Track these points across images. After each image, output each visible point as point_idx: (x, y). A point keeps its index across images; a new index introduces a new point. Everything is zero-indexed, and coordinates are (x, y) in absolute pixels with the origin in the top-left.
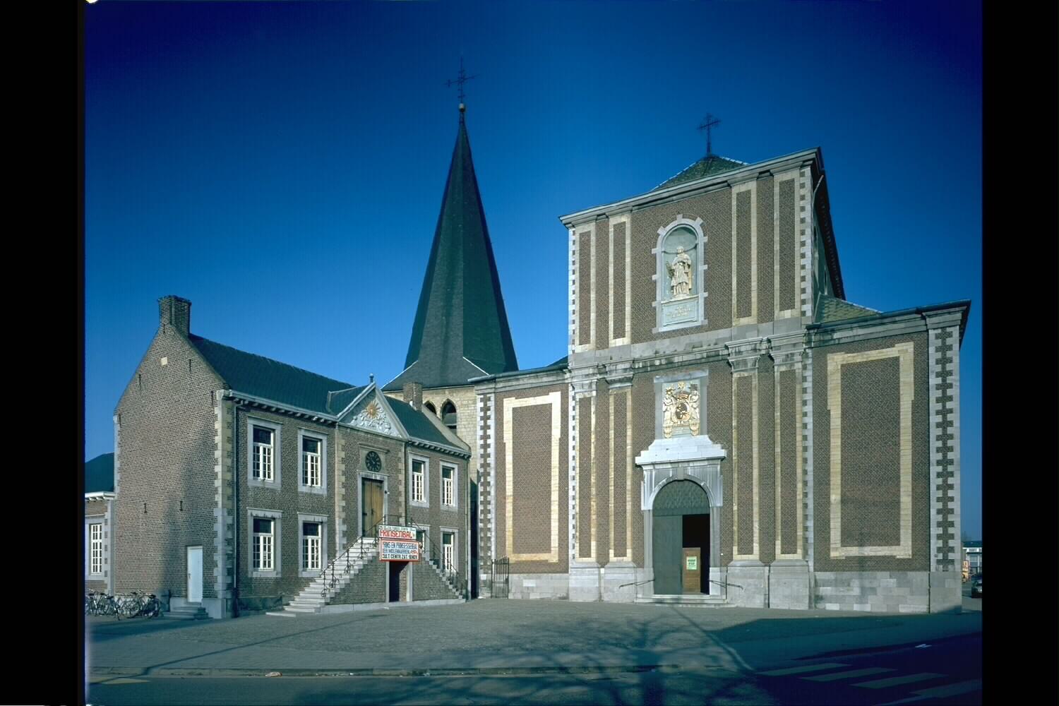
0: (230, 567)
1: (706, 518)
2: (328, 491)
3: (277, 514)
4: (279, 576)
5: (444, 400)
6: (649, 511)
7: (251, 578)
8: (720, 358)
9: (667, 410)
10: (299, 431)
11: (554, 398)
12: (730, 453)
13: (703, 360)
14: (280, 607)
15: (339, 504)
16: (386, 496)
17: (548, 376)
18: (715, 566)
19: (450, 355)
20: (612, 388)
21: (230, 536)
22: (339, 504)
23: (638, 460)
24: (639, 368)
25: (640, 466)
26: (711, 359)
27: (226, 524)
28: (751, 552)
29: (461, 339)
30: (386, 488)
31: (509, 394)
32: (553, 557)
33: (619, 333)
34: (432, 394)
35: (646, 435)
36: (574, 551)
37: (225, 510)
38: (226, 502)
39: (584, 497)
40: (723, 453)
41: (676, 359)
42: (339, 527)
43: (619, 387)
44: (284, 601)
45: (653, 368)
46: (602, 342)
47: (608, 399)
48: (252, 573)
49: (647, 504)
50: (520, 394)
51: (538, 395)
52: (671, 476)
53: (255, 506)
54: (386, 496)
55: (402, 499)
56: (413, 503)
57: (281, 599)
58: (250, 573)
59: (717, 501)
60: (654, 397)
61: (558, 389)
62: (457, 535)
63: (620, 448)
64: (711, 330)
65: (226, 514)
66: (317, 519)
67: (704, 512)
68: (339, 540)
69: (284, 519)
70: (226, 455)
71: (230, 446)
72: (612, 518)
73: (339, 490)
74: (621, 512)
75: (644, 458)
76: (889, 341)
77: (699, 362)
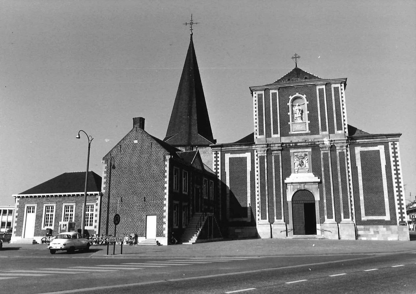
11: (248, 155)
25: (286, 184)
49: (289, 198)
63: (277, 176)
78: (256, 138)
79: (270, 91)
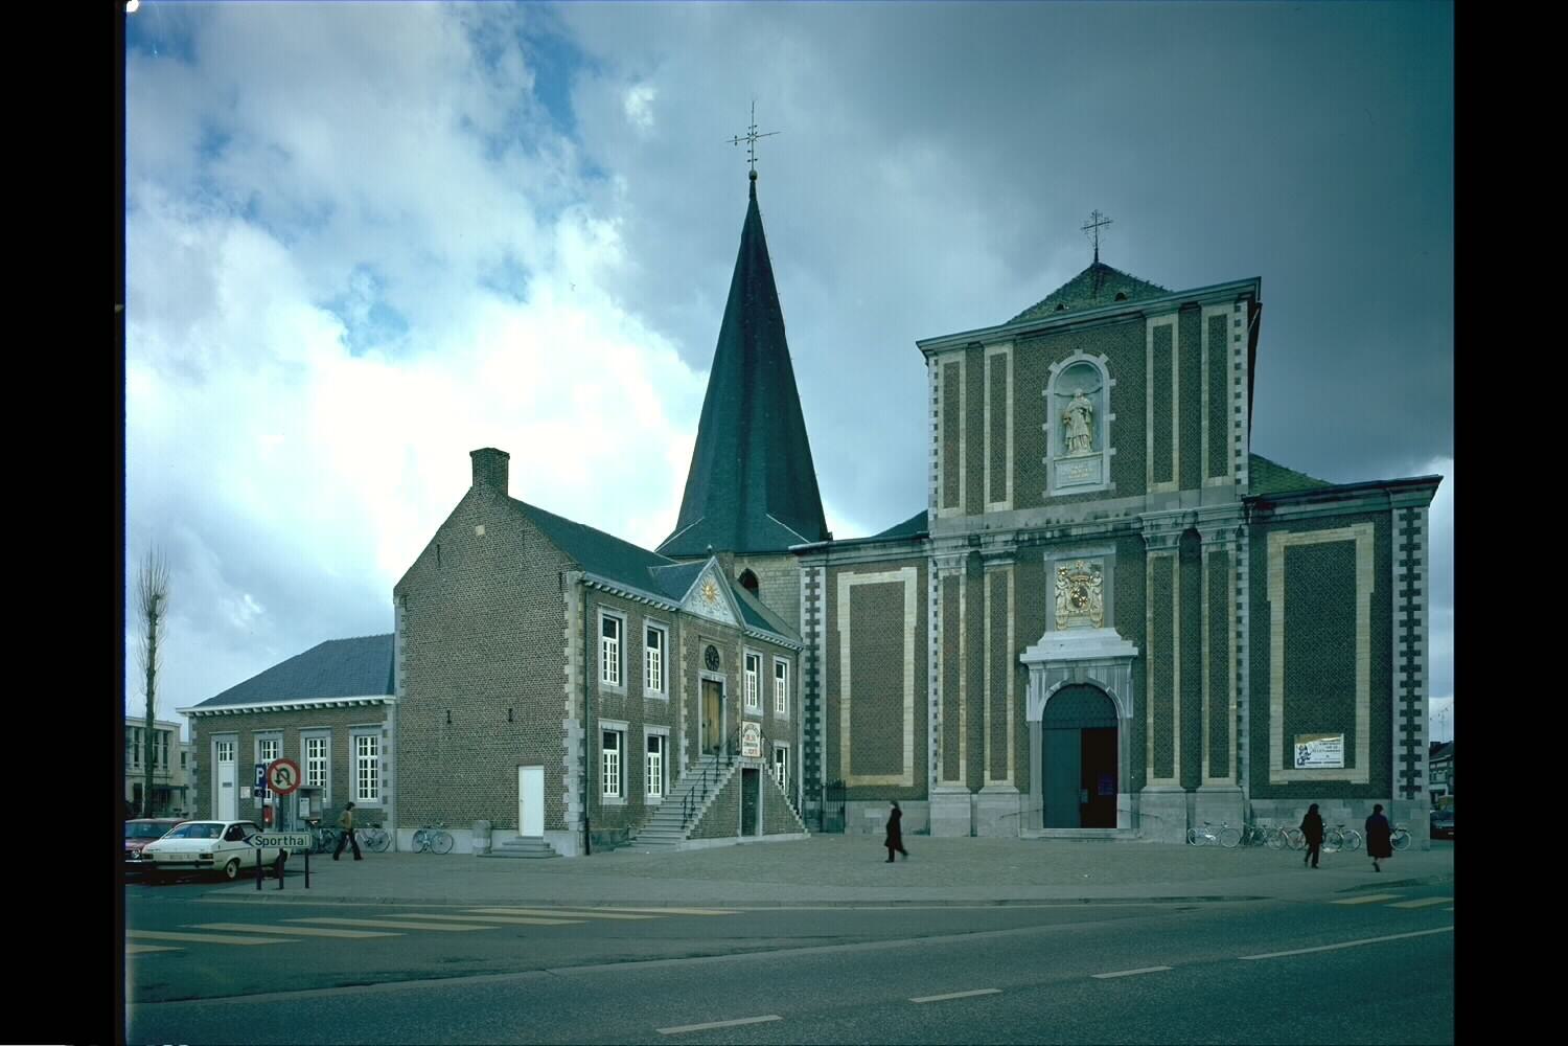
9: (1060, 593)
12: (1143, 653)
25: (1026, 666)
26: (1119, 534)
28: (1170, 775)
31: (846, 567)
35: (1033, 627)
36: (935, 772)
40: (1135, 652)
46: (975, 506)
49: (1035, 711)
59: (1126, 711)
74: (999, 725)
75: (1030, 655)
76: (1344, 520)
78: (936, 516)
79: (1204, 309)
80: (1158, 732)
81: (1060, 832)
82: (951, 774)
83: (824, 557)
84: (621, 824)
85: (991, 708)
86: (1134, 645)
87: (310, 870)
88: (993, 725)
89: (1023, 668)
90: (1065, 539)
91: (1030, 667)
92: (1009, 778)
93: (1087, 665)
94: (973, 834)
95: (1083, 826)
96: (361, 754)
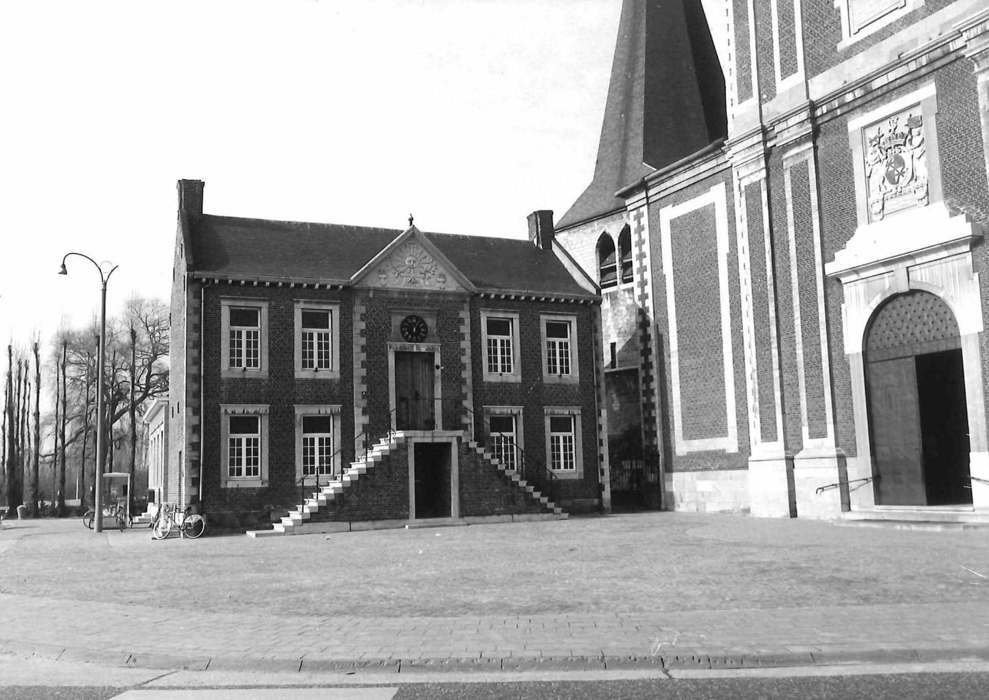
0: (195, 476)
1: (953, 359)
2: (341, 374)
3: (263, 408)
4: (266, 485)
5: (622, 227)
6: (858, 354)
7: (226, 489)
8: (953, 57)
9: (867, 171)
10: (296, 305)
11: (716, 195)
13: (923, 71)
14: (268, 525)
15: (359, 388)
16: (438, 373)
17: (705, 162)
18: (979, 450)
19: (628, 164)
20: (786, 159)
21: (195, 439)
22: (359, 388)
23: (831, 269)
24: (823, 115)
26: (938, 64)
27: (191, 425)
29: (641, 139)
30: (437, 361)
31: (665, 200)
32: (729, 443)
33: (788, 69)
34: (607, 222)
35: (840, 225)
36: (755, 432)
37: (190, 409)
38: (191, 400)
39: (762, 342)
41: (877, 84)
42: (360, 420)
43: (797, 154)
44: (273, 517)
45: (845, 109)
47: (783, 175)
48: (226, 483)
49: (853, 343)
50: (678, 196)
51: (697, 194)
52: (887, 287)
53: (231, 401)
54: (438, 373)
55: (467, 374)
56: (489, 377)
57: (268, 515)
58: (223, 482)
60: (851, 155)
61: (721, 179)
62: (579, 419)
64: (932, 12)
65: (191, 414)
66: (325, 410)
67: (951, 346)
68: (359, 438)
69: (272, 415)
70: (191, 344)
71: (197, 334)
72: (801, 372)
73: (359, 372)
74: (813, 364)
75: (842, 261)
77: (915, 75)
80: (605, 135)
81: (897, 511)
82: (768, 434)
83: (643, 195)
84: (261, 506)
85: (803, 342)
86: (954, 212)
87: (837, 492)
88: (806, 364)
89: (835, 282)
90: (869, 97)
91: (844, 280)
92: (730, 430)
93: (909, 263)
94: (793, 513)
95: (931, 502)
96: (570, 437)
